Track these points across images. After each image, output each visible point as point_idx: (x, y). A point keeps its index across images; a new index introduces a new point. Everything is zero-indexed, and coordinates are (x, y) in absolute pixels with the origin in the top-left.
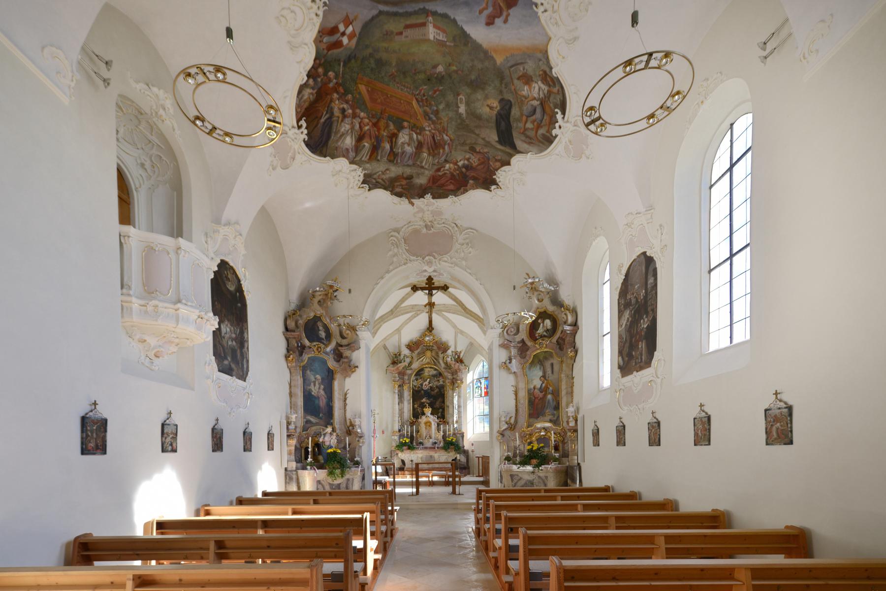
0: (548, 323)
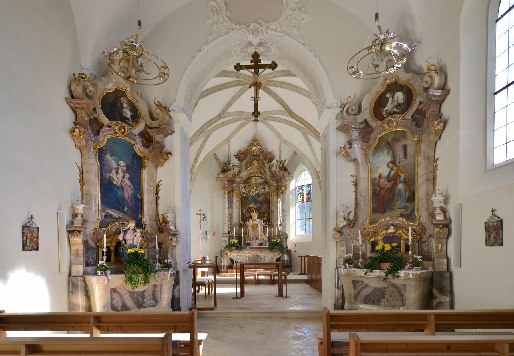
0: (400, 96)
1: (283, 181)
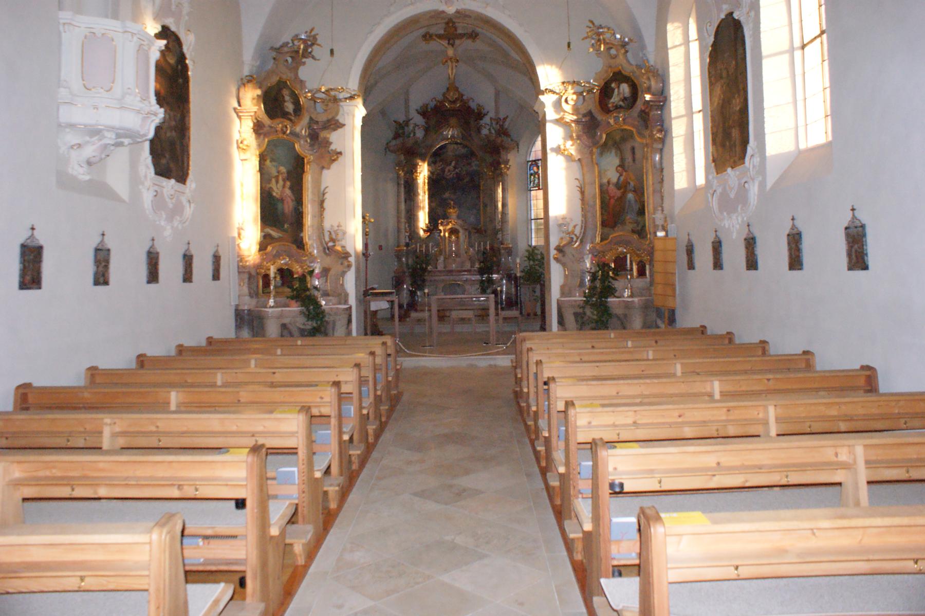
0: (625, 88)
1: (503, 153)
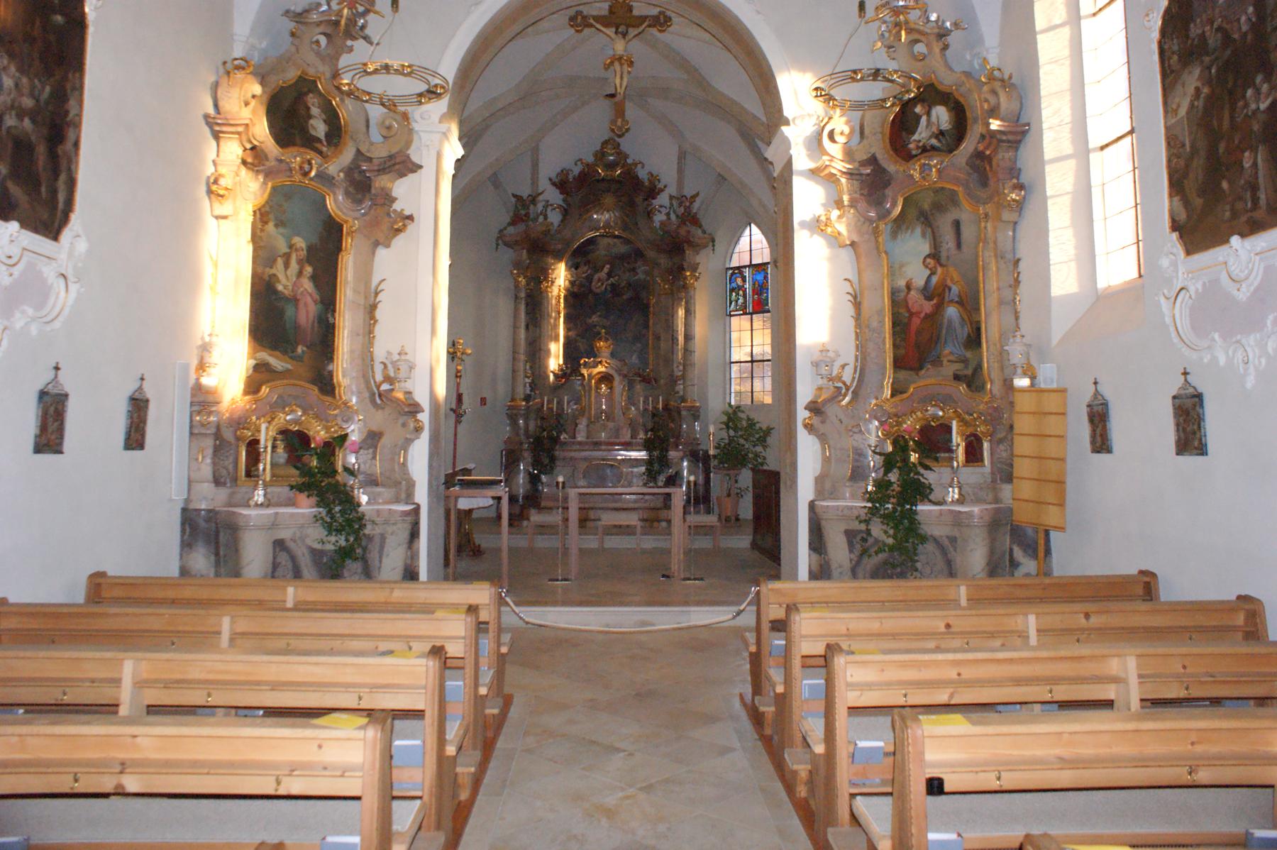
0: (942, 115)
